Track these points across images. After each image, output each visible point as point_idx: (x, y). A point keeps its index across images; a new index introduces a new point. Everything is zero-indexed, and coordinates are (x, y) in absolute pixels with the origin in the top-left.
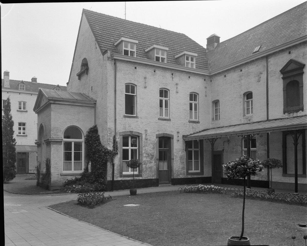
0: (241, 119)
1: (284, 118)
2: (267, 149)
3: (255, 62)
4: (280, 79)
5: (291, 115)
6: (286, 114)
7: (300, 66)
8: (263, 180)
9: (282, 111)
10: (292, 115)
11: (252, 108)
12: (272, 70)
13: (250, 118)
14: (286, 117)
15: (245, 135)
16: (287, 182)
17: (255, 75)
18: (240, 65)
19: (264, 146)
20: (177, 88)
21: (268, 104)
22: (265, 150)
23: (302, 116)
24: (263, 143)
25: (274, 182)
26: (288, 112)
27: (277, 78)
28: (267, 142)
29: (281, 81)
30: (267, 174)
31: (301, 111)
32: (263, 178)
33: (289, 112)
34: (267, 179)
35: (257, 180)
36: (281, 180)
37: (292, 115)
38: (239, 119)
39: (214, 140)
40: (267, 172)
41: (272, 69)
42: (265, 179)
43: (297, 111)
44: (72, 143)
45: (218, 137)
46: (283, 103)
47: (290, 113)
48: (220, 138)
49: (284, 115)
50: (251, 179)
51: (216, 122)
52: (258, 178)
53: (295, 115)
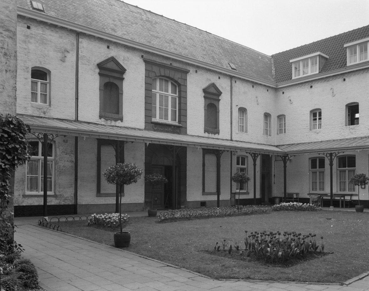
0: (26, 106)
1: (100, 124)
2: (74, 160)
3: (57, 30)
4: (95, 73)
5: (109, 122)
6: (103, 119)
7: (122, 70)
8: (67, 204)
9: (98, 114)
10: (109, 122)
11: (285, 129)
12: (84, 56)
13: (45, 110)
14: (103, 123)
15: (40, 133)
16: (102, 203)
17: (57, 48)
18: (30, 18)
19: (70, 156)
20: (333, 93)
21: (77, 99)
22: (72, 162)
23: (121, 127)
24: (68, 151)
25: (85, 205)
26: (105, 118)
27: (92, 70)
28: (74, 150)
29: (97, 77)
30: (73, 195)
31: (119, 121)
32: (66, 201)
33: (107, 119)
34: (73, 201)
35: (57, 204)
36: (94, 202)
37: (109, 122)
38: (21, 104)
39: (221, 152)
40: (73, 193)
41: (85, 55)
42: (70, 202)
43: (116, 120)
44: (169, 97)
45: (129, 140)
46: (99, 105)
47: (107, 120)
48: (132, 142)
49: (100, 120)
50: (48, 204)
51: (282, 135)
52: (58, 202)
53: (113, 123)
